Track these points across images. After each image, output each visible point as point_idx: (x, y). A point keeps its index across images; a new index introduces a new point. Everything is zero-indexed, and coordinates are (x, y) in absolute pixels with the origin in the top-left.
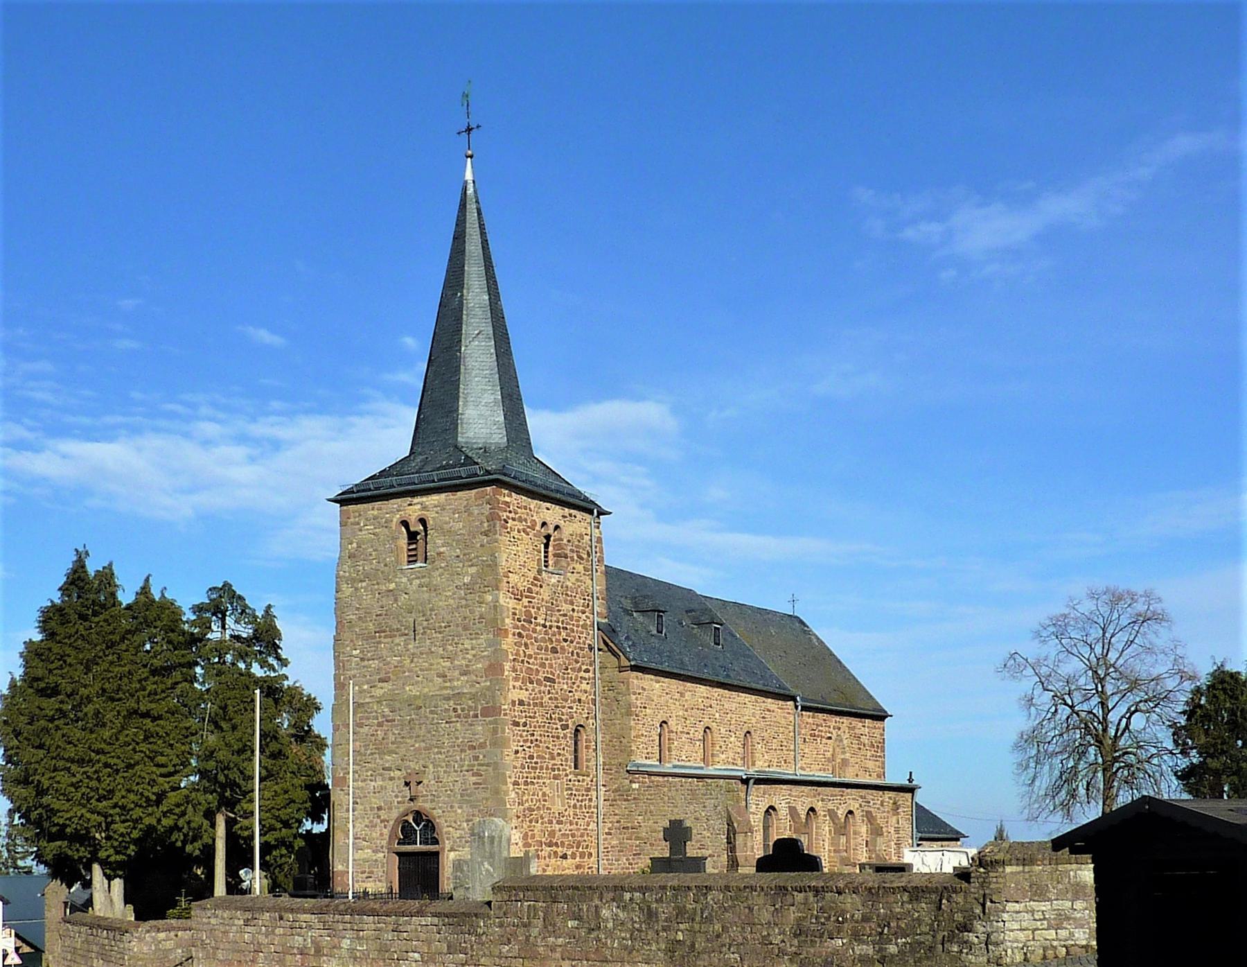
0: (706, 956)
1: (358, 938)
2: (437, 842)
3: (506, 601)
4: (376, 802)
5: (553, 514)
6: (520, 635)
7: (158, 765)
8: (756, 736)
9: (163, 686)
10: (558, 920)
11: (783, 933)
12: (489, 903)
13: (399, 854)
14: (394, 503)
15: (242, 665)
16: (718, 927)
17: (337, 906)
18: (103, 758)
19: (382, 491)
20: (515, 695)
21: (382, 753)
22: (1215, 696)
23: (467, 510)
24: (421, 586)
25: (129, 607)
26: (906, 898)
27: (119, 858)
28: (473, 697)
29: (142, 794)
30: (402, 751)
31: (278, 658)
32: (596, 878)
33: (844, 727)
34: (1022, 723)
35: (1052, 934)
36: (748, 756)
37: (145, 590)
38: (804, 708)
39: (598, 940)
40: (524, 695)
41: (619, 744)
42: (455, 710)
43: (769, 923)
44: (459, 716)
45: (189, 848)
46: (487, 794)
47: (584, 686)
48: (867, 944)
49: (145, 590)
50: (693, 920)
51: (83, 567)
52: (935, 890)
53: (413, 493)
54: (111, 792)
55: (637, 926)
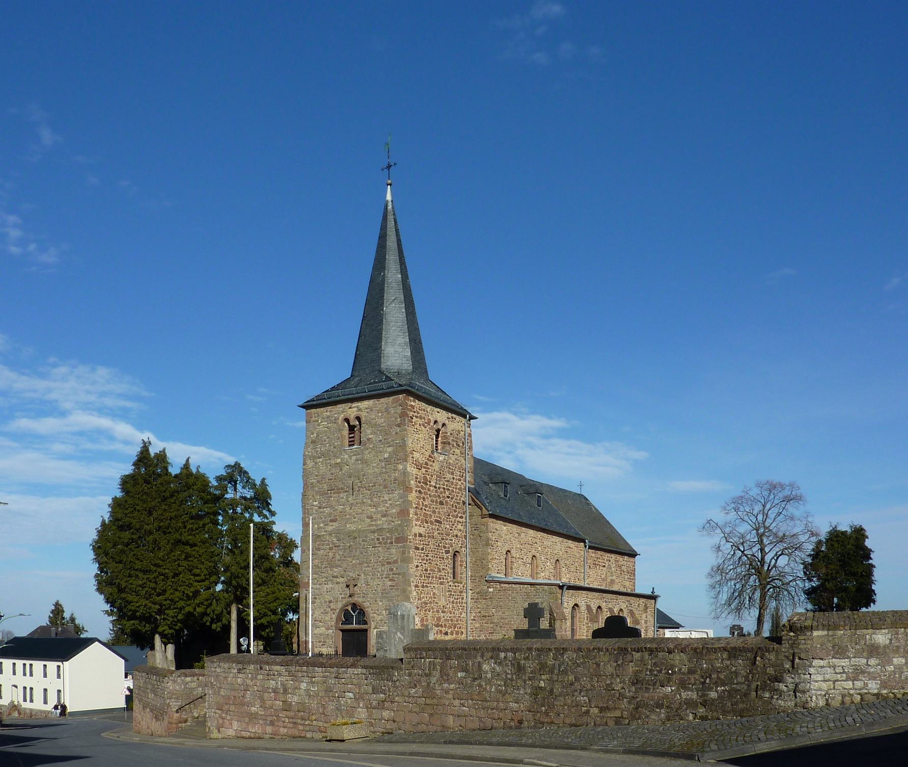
0: (562, 699)
1: (312, 682)
2: (366, 623)
3: (412, 470)
4: (328, 597)
5: (441, 416)
6: (420, 492)
7: (195, 575)
8: (562, 562)
9: (196, 526)
10: (451, 672)
11: (623, 682)
12: (401, 660)
13: (342, 631)
14: (340, 407)
15: (247, 515)
16: (571, 678)
17: (298, 661)
18: (158, 570)
19: (332, 399)
20: (417, 530)
21: (332, 567)
22: (832, 545)
23: (387, 410)
24: (357, 460)
25: (176, 476)
26: (725, 655)
27: (171, 631)
28: (390, 531)
29: (184, 592)
30: (345, 566)
31: (270, 511)
32: (478, 642)
33: (612, 560)
34: (713, 560)
35: (849, 684)
36: (558, 575)
37: (187, 466)
38: (590, 548)
39: (480, 686)
40: (422, 530)
41: (481, 564)
42: (378, 539)
43: (612, 675)
44: (380, 543)
45: (214, 626)
46: (399, 586)
47: (459, 527)
48: (692, 691)
49: (187, 466)
50: (552, 672)
51: (147, 450)
52: (750, 650)
53: (352, 400)
54: (164, 591)
55: (509, 676)
